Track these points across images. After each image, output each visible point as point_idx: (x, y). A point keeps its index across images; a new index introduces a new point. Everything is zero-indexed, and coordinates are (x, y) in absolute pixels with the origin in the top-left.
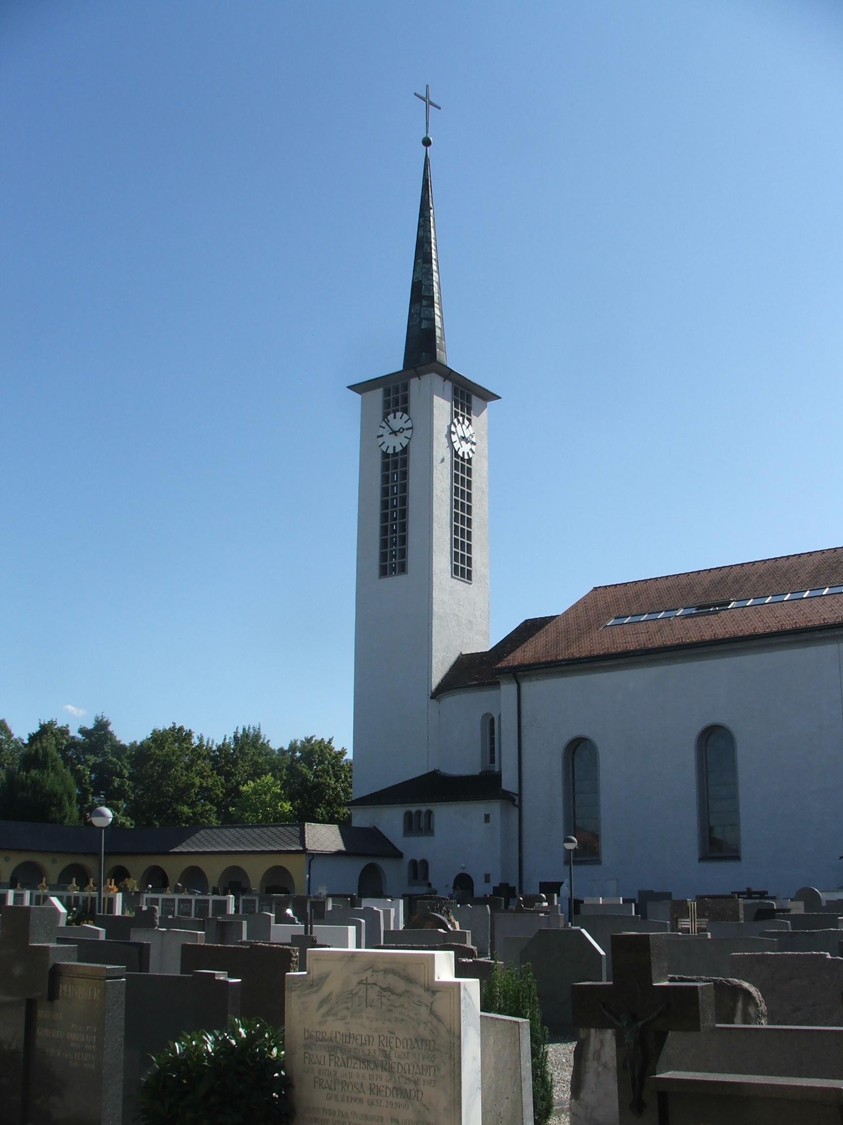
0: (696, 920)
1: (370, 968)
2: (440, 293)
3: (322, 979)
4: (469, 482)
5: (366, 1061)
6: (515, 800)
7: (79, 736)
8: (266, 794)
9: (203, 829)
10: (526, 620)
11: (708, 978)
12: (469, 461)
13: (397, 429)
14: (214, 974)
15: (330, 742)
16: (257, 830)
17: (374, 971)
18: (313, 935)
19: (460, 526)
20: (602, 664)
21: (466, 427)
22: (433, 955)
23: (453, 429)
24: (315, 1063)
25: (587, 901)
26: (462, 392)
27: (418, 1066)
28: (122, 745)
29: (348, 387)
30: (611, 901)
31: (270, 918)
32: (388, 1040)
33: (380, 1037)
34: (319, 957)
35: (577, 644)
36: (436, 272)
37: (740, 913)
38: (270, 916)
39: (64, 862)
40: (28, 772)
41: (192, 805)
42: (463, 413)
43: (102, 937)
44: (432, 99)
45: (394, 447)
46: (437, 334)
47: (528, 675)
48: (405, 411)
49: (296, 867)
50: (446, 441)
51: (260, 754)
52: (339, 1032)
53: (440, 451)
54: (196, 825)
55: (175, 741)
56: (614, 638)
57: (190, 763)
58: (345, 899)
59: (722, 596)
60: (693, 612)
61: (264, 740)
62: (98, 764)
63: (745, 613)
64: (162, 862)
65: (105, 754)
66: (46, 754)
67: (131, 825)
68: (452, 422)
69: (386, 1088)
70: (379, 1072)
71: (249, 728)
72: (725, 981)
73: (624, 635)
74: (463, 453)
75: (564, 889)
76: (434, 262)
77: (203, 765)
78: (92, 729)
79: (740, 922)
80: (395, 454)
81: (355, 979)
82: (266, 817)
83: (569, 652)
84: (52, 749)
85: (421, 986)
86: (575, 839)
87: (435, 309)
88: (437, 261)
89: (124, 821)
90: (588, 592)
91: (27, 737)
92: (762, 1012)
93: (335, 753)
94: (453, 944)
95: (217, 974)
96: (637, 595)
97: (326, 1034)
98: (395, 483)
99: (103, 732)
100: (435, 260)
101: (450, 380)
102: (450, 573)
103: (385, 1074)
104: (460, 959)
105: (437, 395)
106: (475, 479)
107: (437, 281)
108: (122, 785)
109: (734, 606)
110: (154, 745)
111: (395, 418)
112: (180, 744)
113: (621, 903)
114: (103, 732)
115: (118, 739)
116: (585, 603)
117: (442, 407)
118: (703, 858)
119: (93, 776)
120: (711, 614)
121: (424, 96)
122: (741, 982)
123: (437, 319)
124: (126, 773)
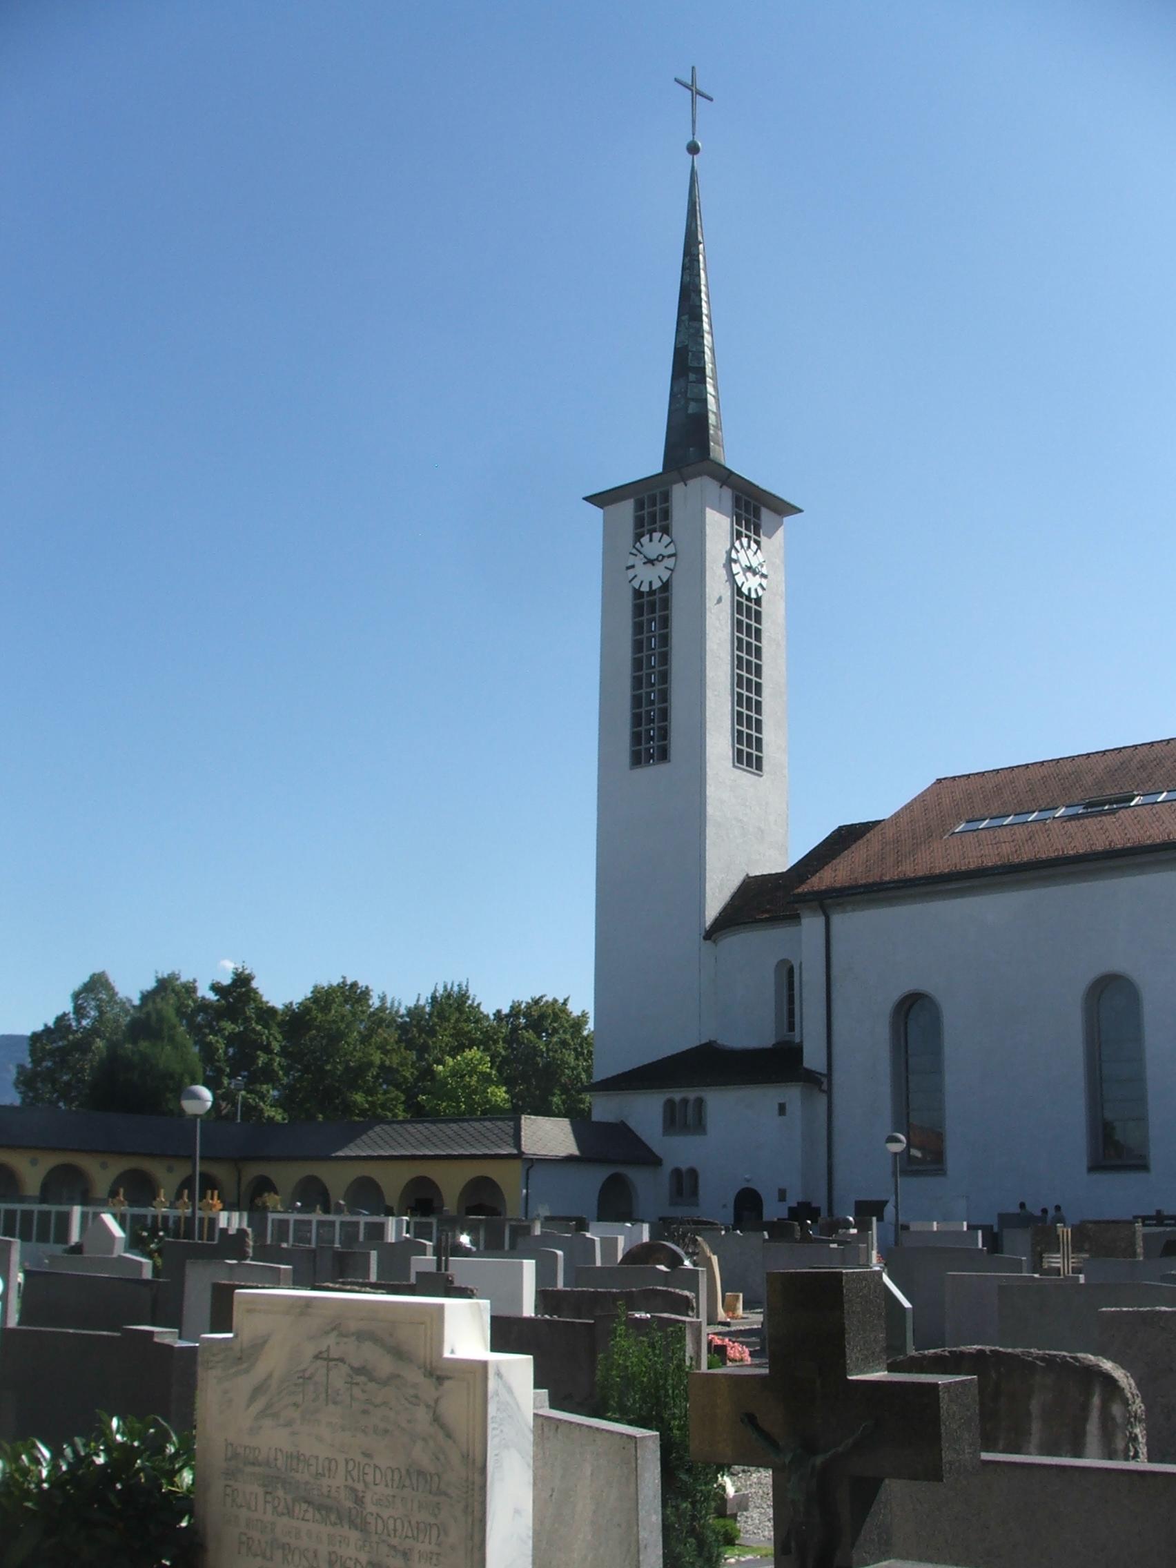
0: (1071, 1256)
1: (333, 1329)
2: (714, 363)
3: (258, 1347)
4: (758, 631)
5: (325, 1508)
6: (822, 1083)
7: (212, 996)
8: (471, 1077)
9: (378, 1124)
10: (840, 827)
11: (1041, 1352)
12: (758, 601)
13: (655, 557)
14: (152, 1333)
15: (565, 1003)
16: (454, 1126)
17: (342, 1335)
18: (449, 1272)
19: (745, 693)
20: (950, 887)
21: (753, 553)
22: (441, 1307)
23: (734, 555)
24: (241, 1506)
25: (915, 1226)
26: (747, 504)
27: (410, 1522)
28: (269, 1007)
29: (586, 499)
30: (951, 1226)
31: (425, 1249)
32: (361, 1468)
33: (347, 1463)
34: (255, 1305)
35: (912, 859)
36: (708, 333)
37: (1137, 1246)
38: (425, 1245)
39: (118, 1166)
40: (135, 1042)
41: (370, 1092)
42: (748, 533)
43: (147, 1274)
44: (700, 86)
45: (651, 583)
46: (710, 421)
47: (839, 905)
48: (666, 530)
49: (507, 1177)
50: (725, 572)
51: (467, 1020)
52: (280, 1450)
53: (716, 587)
54: (373, 1118)
55: (346, 1002)
56: (965, 849)
57: (366, 1033)
58: (565, 1223)
59: (1121, 788)
60: (1080, 812)
61: (473, 1002)
62: (235, 1034)
63: (1155, 812)
64: (323, 1171)
65: (247, 1020)
66: (161, 1019)
67: (284, 1119)
68: (733, 546)
69: (355, 1564)
70: (345, 1530)
71: (452, 984)
72: (1071, 1357)
73: (979, 845)
74: (749, 590)
75: (889, 1210)
76: (705, 319)
77: (386, 1035)
78: (229, 986)
79: (1137, 1259)
80: (652, 592)
81: (310, 1350)
82: (471, 1110)
83: (899, 870)
84: (170, 1013)
85: (419, 1368)
86: (902, 1137)
87: (708, 386)
88: (709, 317)
89: (273, 1113)
90: (929, 785)
91: (139, 996)
92: (1136, 1414)
93: (574, 1019)
94: (659, 1288)
95: (158, 1332)
96: (998, 789)
97: (260, 1452)
98: (651, 634)
99: (244, 990)
100: (707, 316)
101: (729, 486)
102: (731, 761)
103: (354, 1535)
104: (630, 1313)
105: (712, 508)
106: (766, 626)
107: (710, 345)
108: (269, 1064)
109: (1140, 803)
110: (314, 1007)
111: (651, 540)
112: (352, 1006)
113: (965, 1229)
114: (244, 990)
115: (265, 999)
116: (924, 800)
117: (718, 524)
118: (1094, 1168)
119: (231, 1051)
120: (1105, 815)
121: (699, 98)
122: (1098, 1360)
123: (711, 400)
124: (276, 1047)
